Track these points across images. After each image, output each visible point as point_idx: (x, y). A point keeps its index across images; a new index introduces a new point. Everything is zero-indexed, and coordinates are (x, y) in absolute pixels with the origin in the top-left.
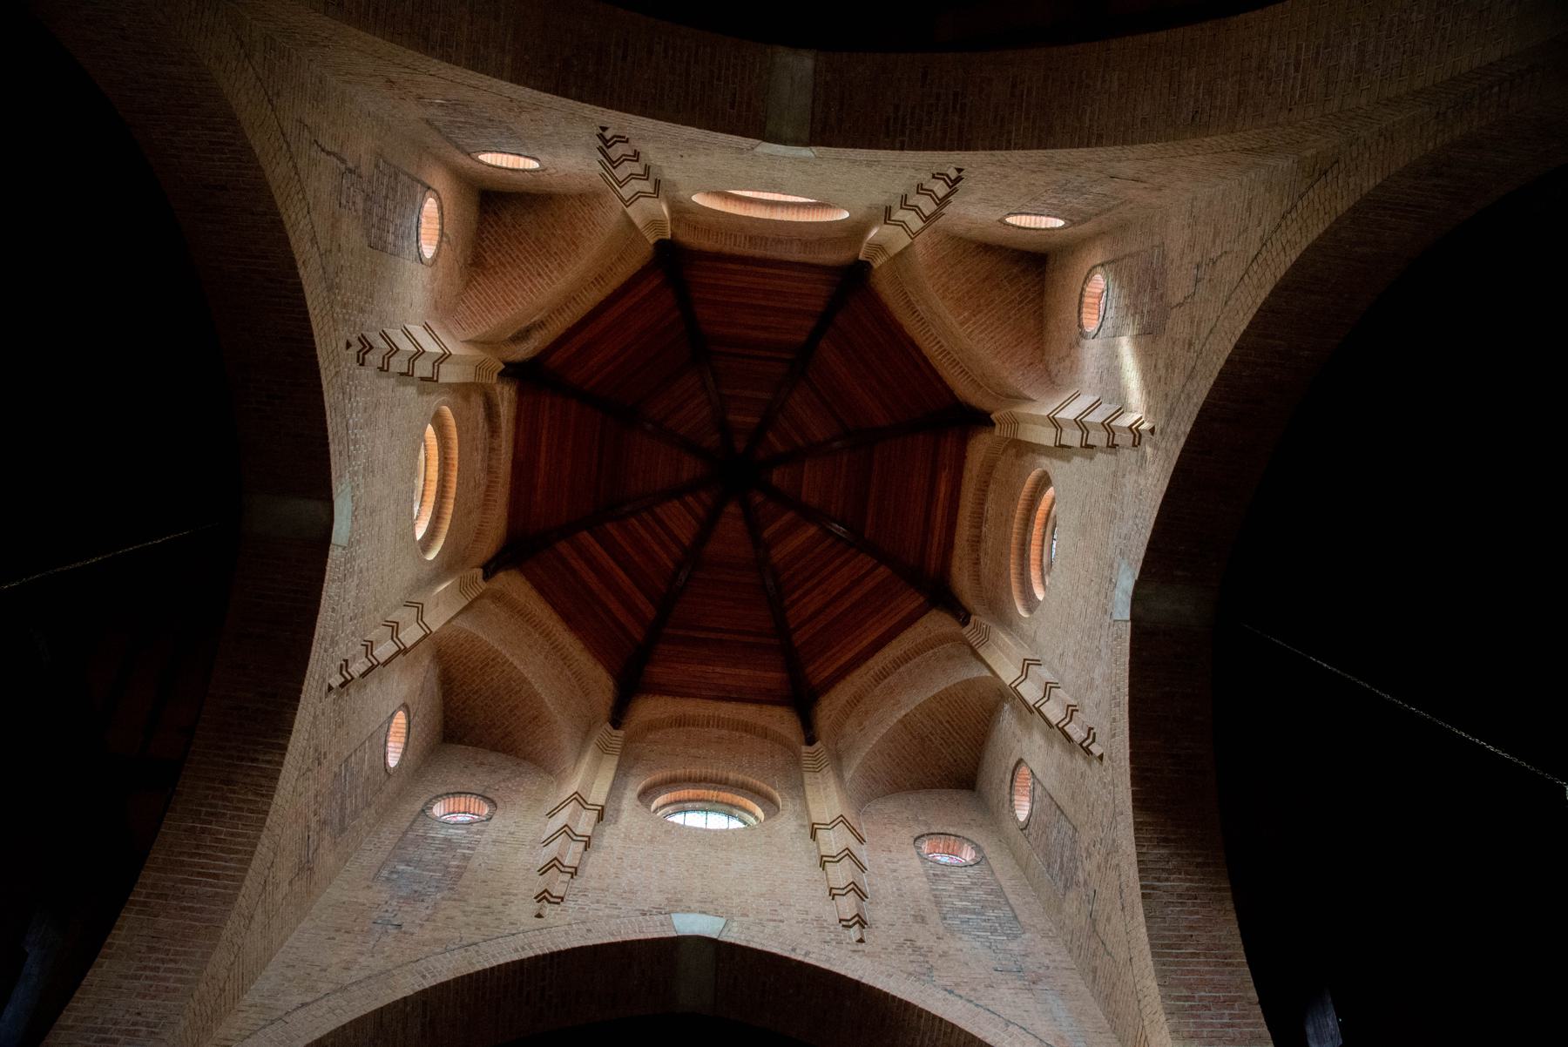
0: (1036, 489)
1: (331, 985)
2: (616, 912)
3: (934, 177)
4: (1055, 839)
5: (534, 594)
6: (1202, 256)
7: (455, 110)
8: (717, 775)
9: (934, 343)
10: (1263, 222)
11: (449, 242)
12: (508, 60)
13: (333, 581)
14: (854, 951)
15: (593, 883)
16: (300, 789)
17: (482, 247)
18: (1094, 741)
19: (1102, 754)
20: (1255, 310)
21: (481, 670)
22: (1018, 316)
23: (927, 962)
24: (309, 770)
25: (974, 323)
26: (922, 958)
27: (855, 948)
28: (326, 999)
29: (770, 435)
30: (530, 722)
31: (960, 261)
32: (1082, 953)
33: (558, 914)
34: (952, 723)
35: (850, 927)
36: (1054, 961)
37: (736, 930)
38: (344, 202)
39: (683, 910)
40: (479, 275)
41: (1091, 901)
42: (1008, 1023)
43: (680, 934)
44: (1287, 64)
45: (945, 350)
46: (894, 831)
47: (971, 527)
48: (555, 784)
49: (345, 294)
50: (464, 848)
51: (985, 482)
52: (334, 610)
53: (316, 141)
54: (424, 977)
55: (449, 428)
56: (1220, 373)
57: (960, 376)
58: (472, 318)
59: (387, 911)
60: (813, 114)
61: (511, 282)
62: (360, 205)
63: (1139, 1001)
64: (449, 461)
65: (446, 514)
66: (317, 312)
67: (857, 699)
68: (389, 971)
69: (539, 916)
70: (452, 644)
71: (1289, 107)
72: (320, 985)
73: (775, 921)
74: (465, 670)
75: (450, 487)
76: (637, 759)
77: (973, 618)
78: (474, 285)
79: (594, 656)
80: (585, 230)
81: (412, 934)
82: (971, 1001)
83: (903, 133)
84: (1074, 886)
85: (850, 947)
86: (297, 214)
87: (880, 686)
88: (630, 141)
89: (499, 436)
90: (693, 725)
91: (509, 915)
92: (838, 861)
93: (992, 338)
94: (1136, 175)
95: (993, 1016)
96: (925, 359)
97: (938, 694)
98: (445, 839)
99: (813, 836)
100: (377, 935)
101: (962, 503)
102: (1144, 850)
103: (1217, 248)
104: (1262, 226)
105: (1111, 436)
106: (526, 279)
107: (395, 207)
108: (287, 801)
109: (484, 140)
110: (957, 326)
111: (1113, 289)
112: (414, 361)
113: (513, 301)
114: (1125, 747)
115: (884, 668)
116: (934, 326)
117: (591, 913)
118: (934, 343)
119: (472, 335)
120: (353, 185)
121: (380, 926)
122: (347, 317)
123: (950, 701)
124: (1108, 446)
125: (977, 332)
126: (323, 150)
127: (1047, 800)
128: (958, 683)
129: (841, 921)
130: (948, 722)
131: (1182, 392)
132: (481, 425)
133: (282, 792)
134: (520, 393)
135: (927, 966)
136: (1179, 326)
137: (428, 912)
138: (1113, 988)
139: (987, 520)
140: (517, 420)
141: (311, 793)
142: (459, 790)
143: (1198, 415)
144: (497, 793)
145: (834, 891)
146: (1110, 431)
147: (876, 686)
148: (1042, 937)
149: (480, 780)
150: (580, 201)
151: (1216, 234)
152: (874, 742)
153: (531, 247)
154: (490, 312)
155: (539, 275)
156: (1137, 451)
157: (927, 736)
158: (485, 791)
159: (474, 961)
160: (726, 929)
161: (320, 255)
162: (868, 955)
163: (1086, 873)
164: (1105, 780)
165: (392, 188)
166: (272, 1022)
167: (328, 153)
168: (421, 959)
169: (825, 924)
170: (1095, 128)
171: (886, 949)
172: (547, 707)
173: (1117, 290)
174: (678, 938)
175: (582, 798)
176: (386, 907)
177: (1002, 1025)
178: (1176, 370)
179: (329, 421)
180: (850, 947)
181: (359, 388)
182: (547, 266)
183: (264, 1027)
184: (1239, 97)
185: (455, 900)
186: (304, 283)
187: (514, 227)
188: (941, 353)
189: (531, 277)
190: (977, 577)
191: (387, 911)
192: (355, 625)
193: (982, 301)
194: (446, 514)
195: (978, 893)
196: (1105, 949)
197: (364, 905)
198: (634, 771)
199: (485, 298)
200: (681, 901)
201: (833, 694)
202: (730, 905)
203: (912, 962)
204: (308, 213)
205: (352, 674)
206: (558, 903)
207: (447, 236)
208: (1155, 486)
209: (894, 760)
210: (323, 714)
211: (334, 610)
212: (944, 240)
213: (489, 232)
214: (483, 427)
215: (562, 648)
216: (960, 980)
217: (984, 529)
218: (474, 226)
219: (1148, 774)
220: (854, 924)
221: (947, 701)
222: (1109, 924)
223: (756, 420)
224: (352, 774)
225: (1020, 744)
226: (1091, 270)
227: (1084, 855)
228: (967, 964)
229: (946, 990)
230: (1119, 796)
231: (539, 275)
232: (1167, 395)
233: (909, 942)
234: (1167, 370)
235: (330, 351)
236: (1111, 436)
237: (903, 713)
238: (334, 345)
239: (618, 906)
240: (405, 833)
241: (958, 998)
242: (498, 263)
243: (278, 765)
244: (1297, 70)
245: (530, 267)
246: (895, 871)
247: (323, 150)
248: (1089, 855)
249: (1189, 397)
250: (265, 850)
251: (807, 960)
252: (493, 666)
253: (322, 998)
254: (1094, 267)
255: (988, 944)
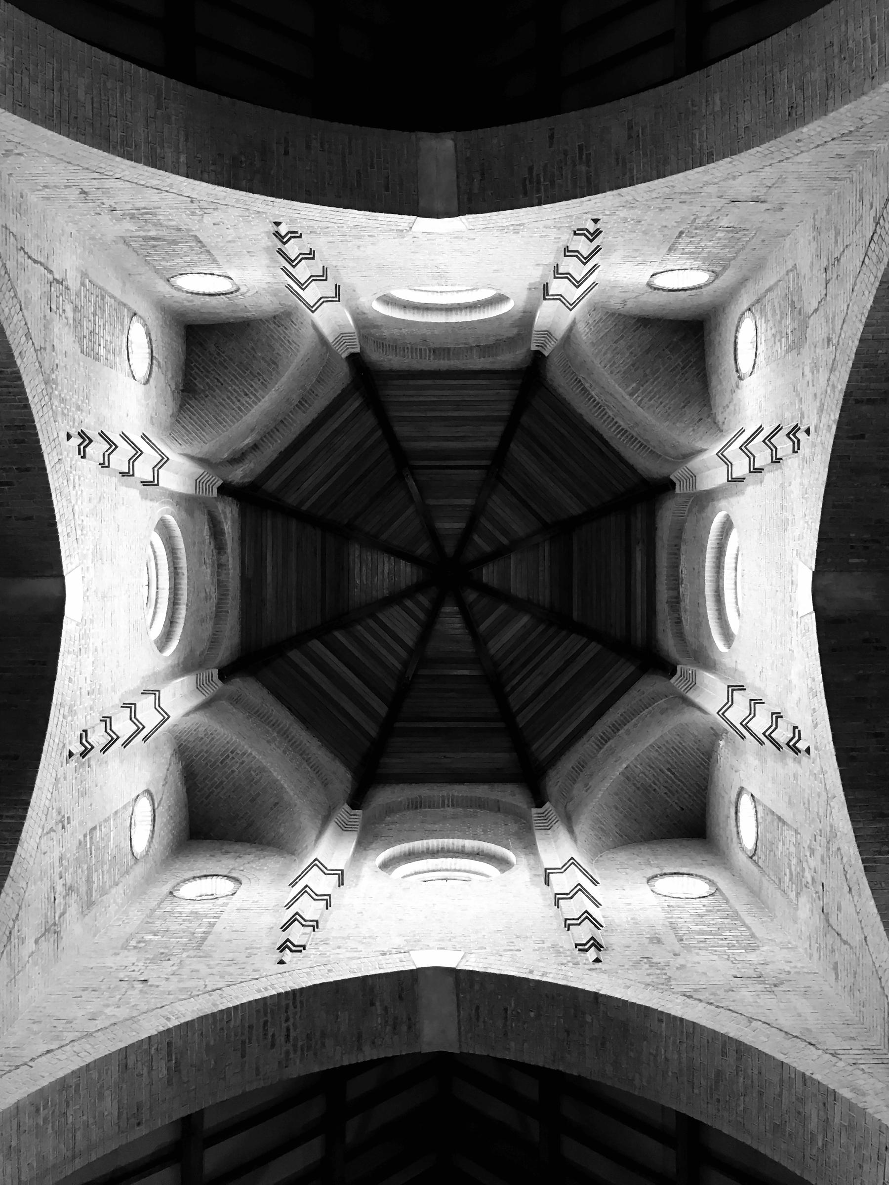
0: (722, 535)
1: (77, 1034)
2: (356, 955)
3: (575, 234)
4: (782, 853)
5: (270, 698)
6: (828, 260)
7: (146, 221)
8: (453, 844)
9: (612, 424)
10: (874, 205)
11: (159, 366)
12: (183, 158)
13: (69, 652)
14: (590, 970)
15: (334, 934)
16: (43, 847)
17: (191, 375)
18: (800, 739)
19: (809, 747)
20: (877, 284)
21: (221, 763)
22: (683, 380)
23: (665, 974)
24: (52, 830)
25: (642, 393)
26: (659, 972)
27: (593, 966)
28: (71, 1045)
29: (476, 537)
30: (272, 809)
31: (622, 337)
32: (822, 954)
33: (300, 960)
34: (673, 770)
35: (587, 950)
36: (795, 967)
37: (474, 960)
38: (54, 307)
39: (421, 949)
40: (191, 399)
41: (821, 897)
42: (751, 1019)
43: (418, 967)
44: (864, 40)
45: (623, 429)
46: (627, 874)
47: (668, 589)
48: (297, 861)
49: (62, 390)
50: (210, 918)
51: (676, 546)
52: (70, 680)
53: (22, 248)
54: (168, 1019)
55: (176, 538)
56: (856, 354)
57: (639, 450)
58: (187, 436)
59: (134, 971)
60: (458, 187)
61: (221, 403)
62: (70, 314)
63: (880, 979)
64: (179, 571)
65: (179, 618)
66: (36, 400)
67: (582, 766)
68: (134, 1017)
69: (281, 962)
70: (191, 739)
71: (871, 76)
72: (65, 1034)
73: (511, 950)
74: (207, 764)
75: (182, 595)
76: (376, 836)
77: (679, 668)
78: (187, 408)
79: (332, 752)
80: (281, 349)
81: (157, 986)
82: (711, 1004)
83: (538, 191)
84: (804, 889)
85: (587, 967)
86: (10, 310)
87: (602, 751)
88: (303, 236)
89: (225, 553)
90: (429, 807)
91: (253, 964)
92: (571, 898)
93: (661, 403)
94: (756, 194)
95: (735, 1015)
96: (606, 443)
97: (655, 743)
98: (192, 913)
99: (557, 904)
100: (124, 990)
101: (658, 570)
102: (861, 825)
103: (839, 245)
104: (874, 208)
105: (774, 452)
106: (234, 400)
107: (104, 325)
108: (31, 856)
109: (178, 260)
110: (627, 397)
111: (761, 326)
112: (134, 462)
113: (224, 419)
114: (826, 730)
115: (604, 733)
116: (610, 409)
117: (332, 956)
118: (612, 424)
119: (189, 451)
120: (61, 294)
121: (127, 983)
122: (66, 411)
123: (668, 749)
124: (772, 462)
125: (646, 400)
126: (29, 257)
127: (769, 818)
128: (672, 729)
129: (576, 945)
130: (669, 770)
131: (828, 385)
132: (207, 541)
133: (25, 845)
134: (242, 514)
135: (664, 977)
136: (818, 329)
137: (174, 968)
138: (855, 977)
139: (683, 580)
140: (242, 540)
141: (56, 855)
142: (205, 873)
143: (843, 399)
144: (242, 873)
145: (568, 922)
146: (772, 447)
147: (598, 752)
148: (781, 948)
149: (225, 864)
150: (275, 323)
151: (837, 234)
152: (600, 796)
153: (236, 370)
154: (203, 430)
155: (246, 395)
156: (799, 456)
157: (650, 786)
158: (229, 872)
159: (218, 1003)
160: (464, 960)
161: (36, 350)
162: (605, 972)
163: (813, 870)
164: (815, 772)
165: (100, 307)
166: (17, 1067)
167: (35, 262)
168: (166, 1005)
169: (561, 950)
170: (705, 147)
171: (623, 966)
172: (287, 792)
173: (764, 325)
174: (418, 970)
175: (321, 864)
176: (133, 968)
177: (745, 1022)
178: (821, 369)
179: (55, 503)
180: (587, 967)
181: (82, 479)
182: (252, 386)
183: (10, 1071)
184: (827, 82)
185: (200, 957)
186: (22, 371)
187: (218, 354)
188: (619, 432)
189: (239, 398)
190: (680, 635)
191: (134, 971)
192: (94, 700)
193: (648, 371)
194: (179, 618)
195: (715, 918)
196: (841, 939)
197: (111, 968)
198: (373, 846)
199: (198, 418)
200: (419, 941)
201: (559, 765)
202: (468, 941)
203: (649, 975)
204: (21, 310)
205: (92, 743)
206: (300, 951)
207: (157, 360)
208: (817, 480)
209: (621, 813)
210: (65, 779)
211: (70, 680)
212: (604, 318)
213: (197, 361)
214: (210, 543)
215: (300, 745)
216: (699, 987)
217: (681, 590)
218: (183, 357)
219: (854, 754)
220: (590, 947)
221: (664, 748)
222: (840, 911)
223: (462, 525)
224: (97, 849)
225: (738, 774)
226: (740, 318)
227: (808, 854)
228: (705, 974)
229: (684, 995)
230: (829, 782)
231: (246, 395)
232: (815, 395)
233: (645, 960)
234: (813, 373)
235: (51, 439)
236: (774, 452)
237: (624, 766)
238: (55, 435)
239: (359, 949)
240: (153, 911)
241: (697, 1002)
242: (207, 388)
243: (21, 819)
244: (873, 42)
245: (237, 388)
246: (629, 904)
247: (29, 257)
248: (812, 851)
249: (834, 387)
250: (8, 900)
251: (544, 979)
252: (233, 758)
253: (67, 1045)
254: (743, 314)
255: (726, 957)
